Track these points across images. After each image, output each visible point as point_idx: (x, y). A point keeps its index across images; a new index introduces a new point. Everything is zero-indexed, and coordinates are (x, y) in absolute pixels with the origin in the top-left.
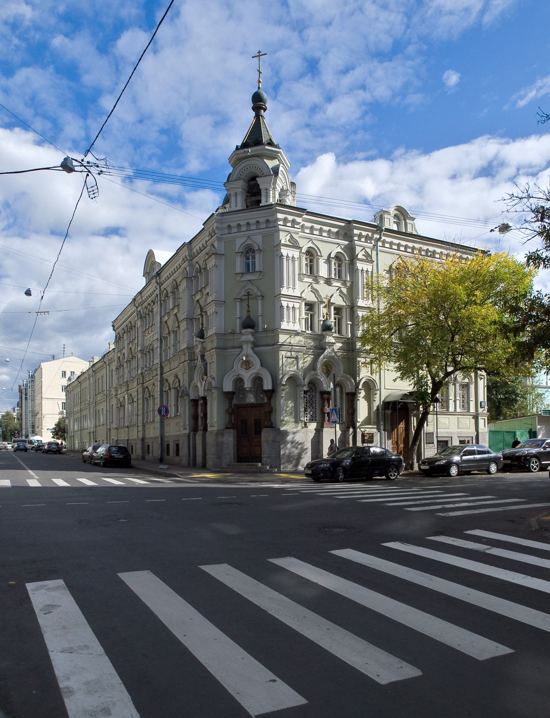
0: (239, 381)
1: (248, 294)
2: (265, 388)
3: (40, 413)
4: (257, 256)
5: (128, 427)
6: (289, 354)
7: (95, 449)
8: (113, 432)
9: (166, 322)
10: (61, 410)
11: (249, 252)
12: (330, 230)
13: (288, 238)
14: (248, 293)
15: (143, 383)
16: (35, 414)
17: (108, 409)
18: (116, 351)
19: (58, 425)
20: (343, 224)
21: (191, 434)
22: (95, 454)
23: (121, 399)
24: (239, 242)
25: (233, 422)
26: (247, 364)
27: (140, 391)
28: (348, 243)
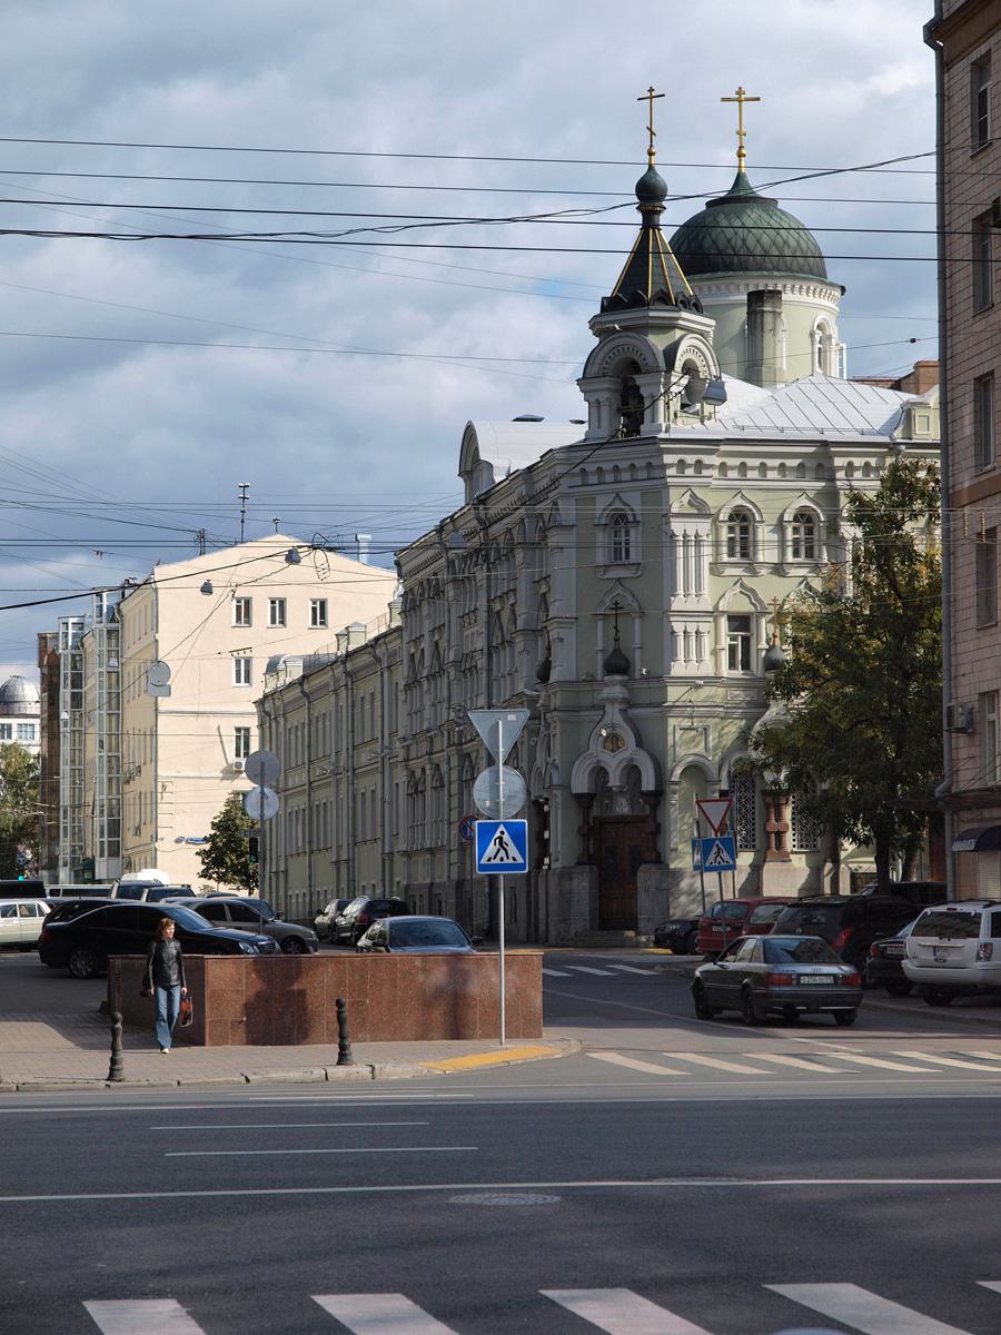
0: (600, 773)
1: (617, 606)
2: (644, 788)
3: (147, 771)
4: (632, 532)
5: (431, 851)
6: (687, 723)
7: (341, 907)
8: (400, 862)
9: (498, 612)
10: (232, 758)
11: (619, 521)
12: (782, 465)
13: (687, 498)
14: (617, 603)
15: (461, 744)
16: (120, 774)
17: (387, 798)
18: (406, 636)
19: (226, 826)
20: (811, 450)
21: (533, 874)
22: (342, 921)
23: (418, 774)
24: (602, 506)
25: (592, 851)
26: (614, 741)
27: (454, 762)
28: (823, 484)
